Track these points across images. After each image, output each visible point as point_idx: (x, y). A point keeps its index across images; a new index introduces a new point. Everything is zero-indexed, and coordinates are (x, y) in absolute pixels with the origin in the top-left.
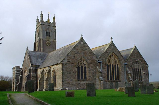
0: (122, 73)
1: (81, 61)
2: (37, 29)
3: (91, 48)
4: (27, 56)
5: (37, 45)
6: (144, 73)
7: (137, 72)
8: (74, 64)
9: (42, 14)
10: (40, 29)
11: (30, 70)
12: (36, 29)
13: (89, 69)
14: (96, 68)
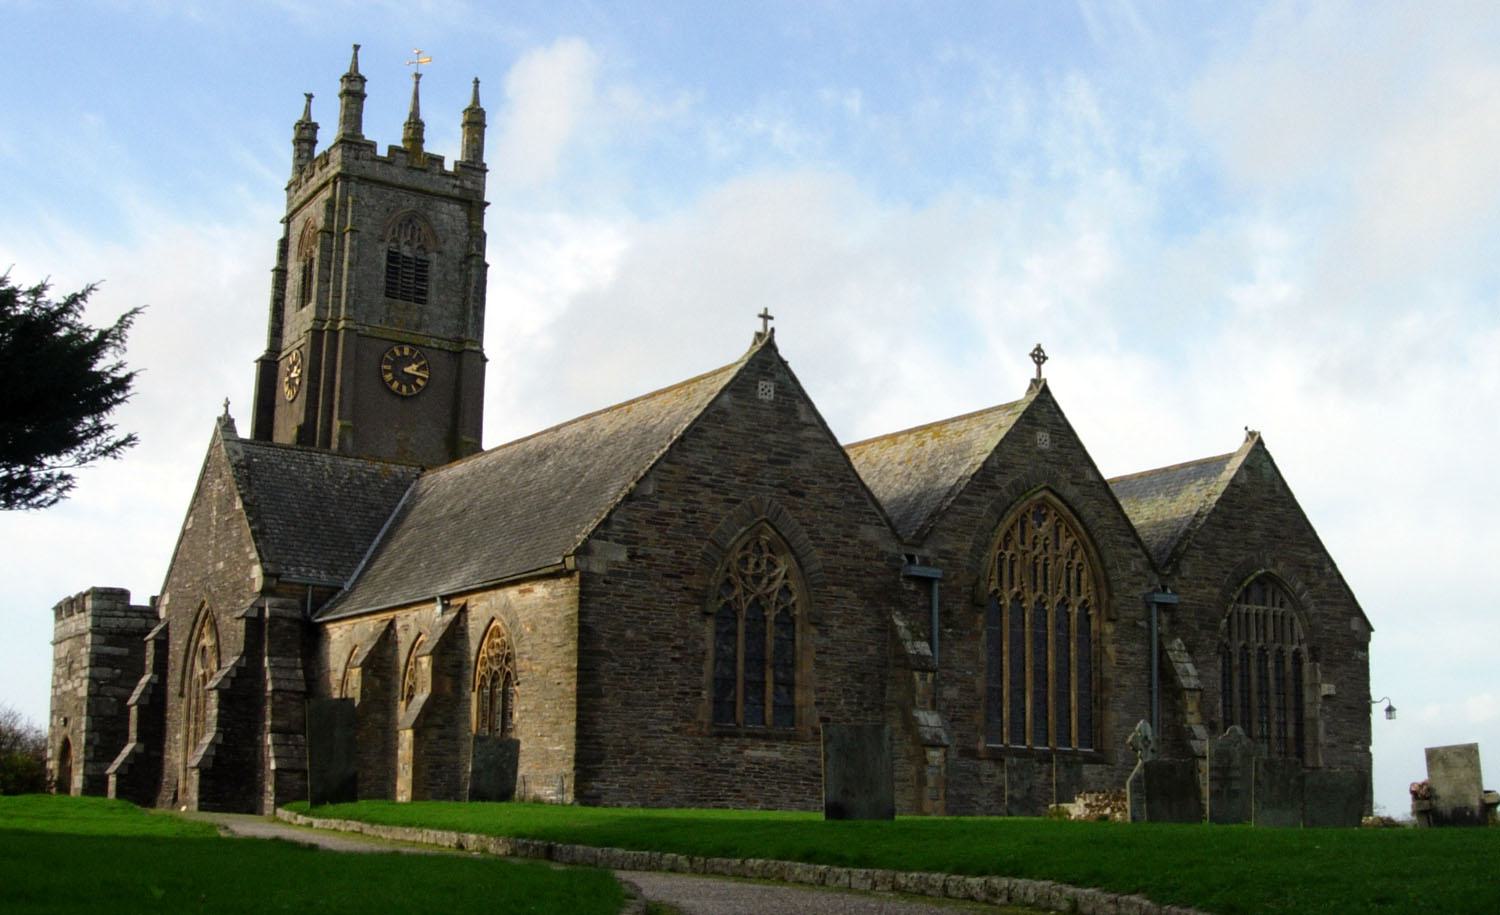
0: (1127, 681)
1: (752, 561)
2: (298, 224)
3: (843, 441)
4: (217, 487)
5: (291, 383)
6: (1327, 697)
7: (1263, 678)
8: (687, 581)
9: (362, 71)
10: (329, 220)
11: (254, 625)
12: (288, 221)
13: (824, 633)
14: (888, 628)
